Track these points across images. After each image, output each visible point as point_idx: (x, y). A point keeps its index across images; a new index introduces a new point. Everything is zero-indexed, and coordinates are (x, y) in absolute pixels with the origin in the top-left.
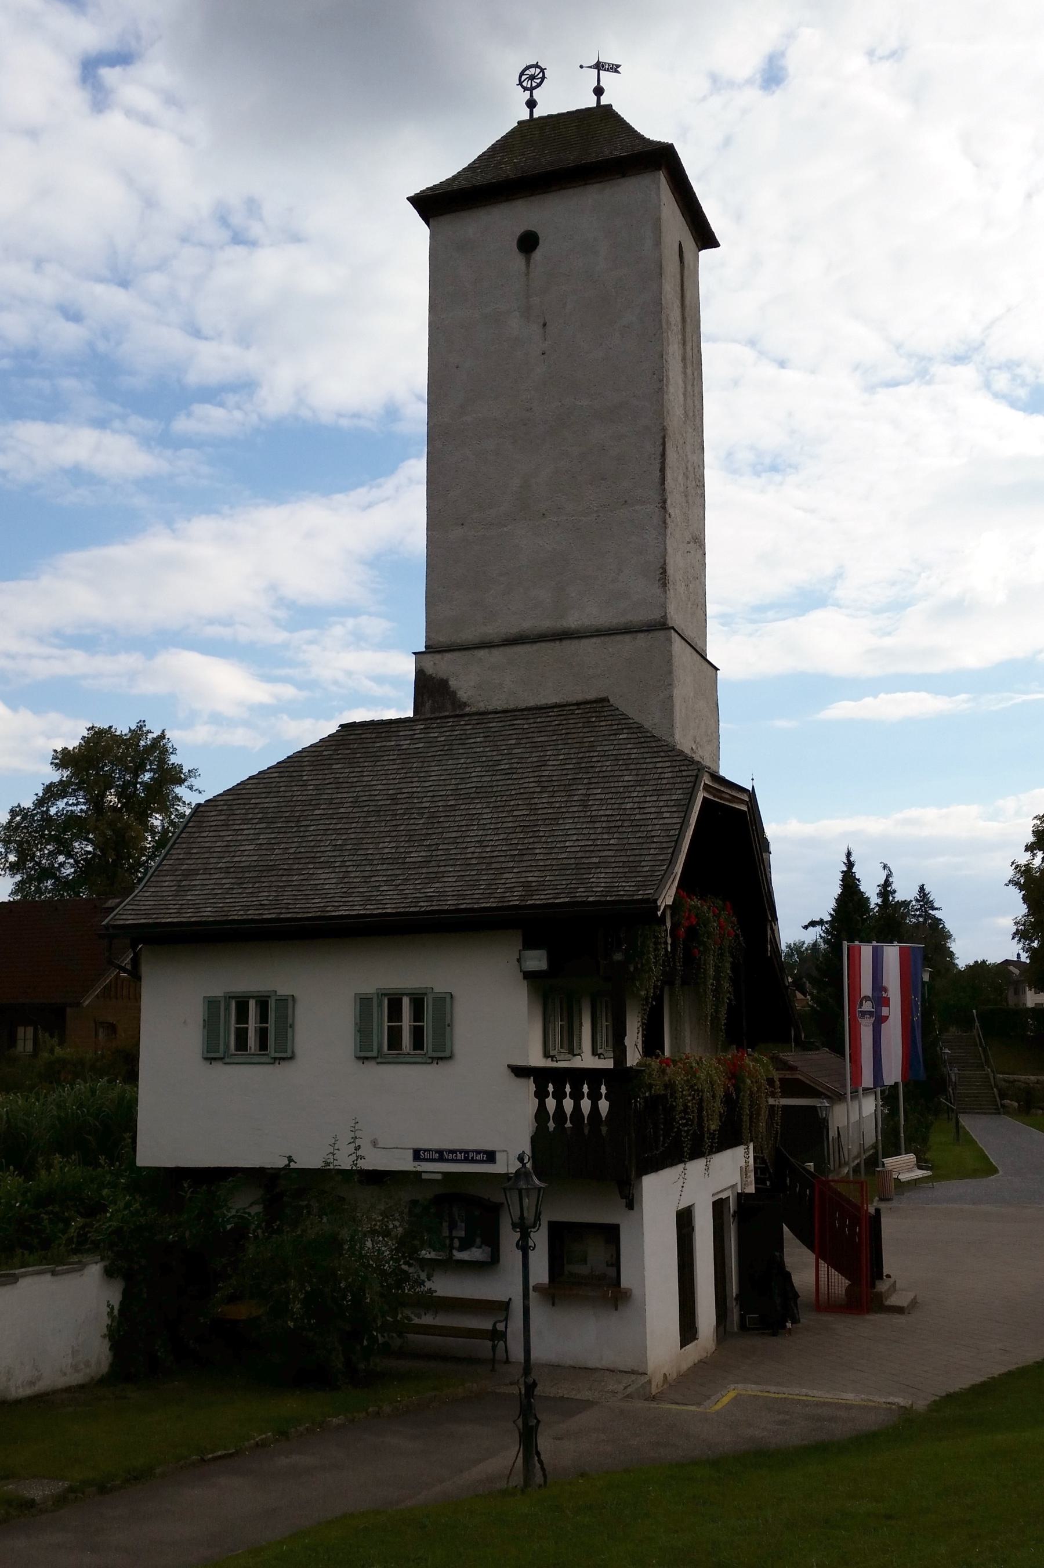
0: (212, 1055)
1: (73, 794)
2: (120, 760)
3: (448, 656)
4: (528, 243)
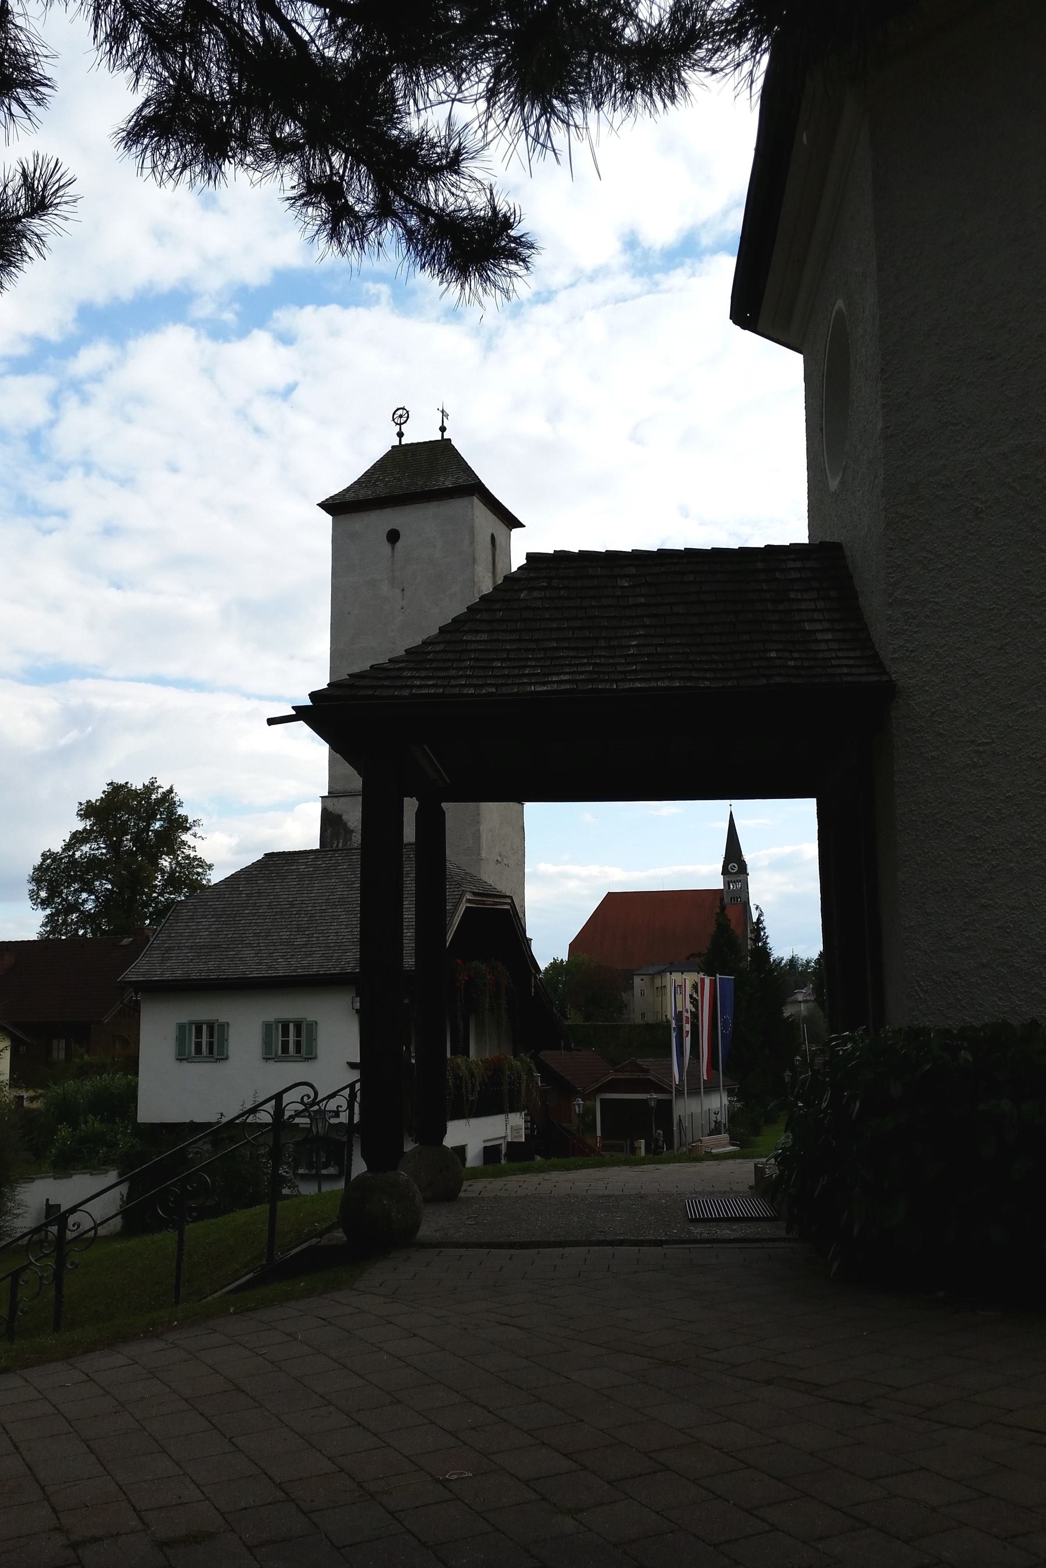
0: (182, 1057)
1: (96, 840)
2: (131, 811)
3: (342, 799)
4: (393, 537)
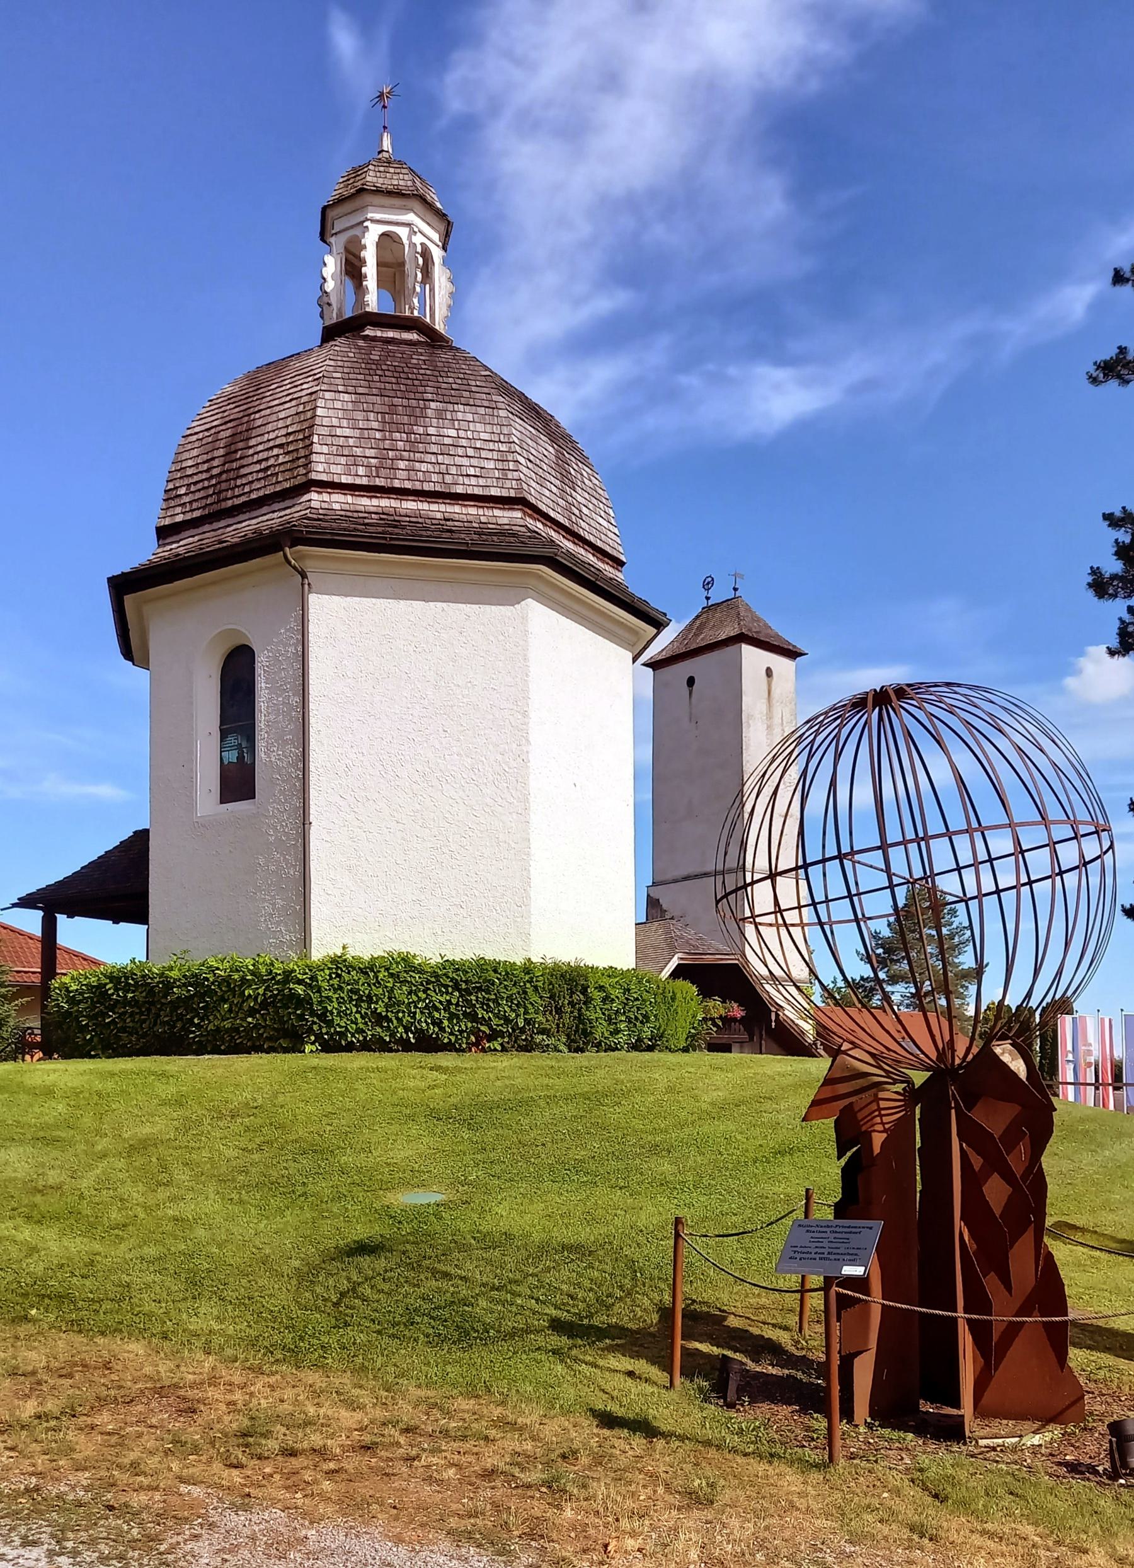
4: (691, 682)
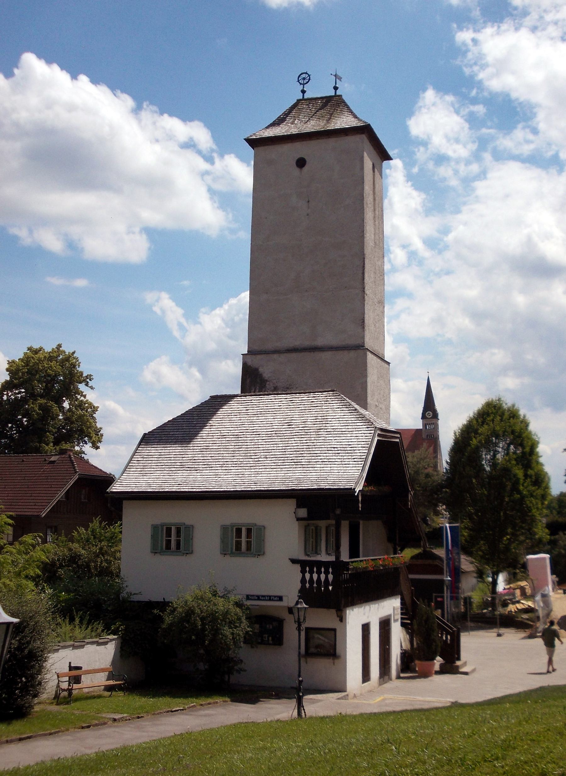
3: (259, 357)
4: (301, 163)
